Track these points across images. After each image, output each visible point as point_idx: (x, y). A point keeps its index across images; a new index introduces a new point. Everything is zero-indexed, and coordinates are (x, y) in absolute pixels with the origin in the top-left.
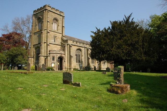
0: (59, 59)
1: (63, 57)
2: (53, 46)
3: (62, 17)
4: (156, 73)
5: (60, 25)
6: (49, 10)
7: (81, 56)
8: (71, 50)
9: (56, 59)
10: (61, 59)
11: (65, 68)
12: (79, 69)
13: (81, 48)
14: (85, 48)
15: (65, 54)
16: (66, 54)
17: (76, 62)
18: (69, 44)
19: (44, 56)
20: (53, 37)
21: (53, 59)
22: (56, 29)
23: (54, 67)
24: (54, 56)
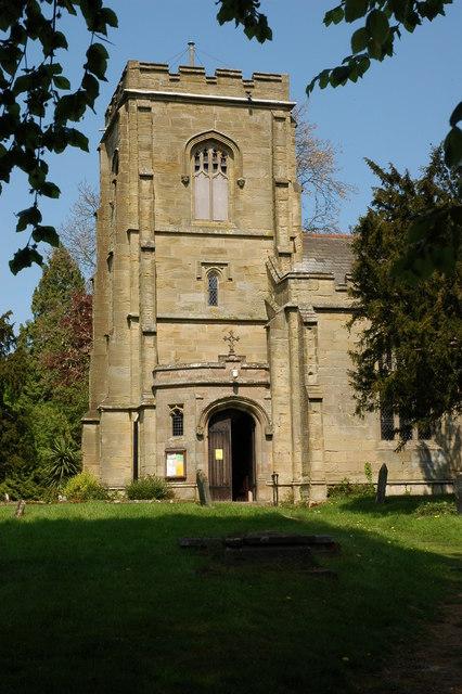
0: (225, 425)
1: (250, 408)
2: (203, 336)
3: (264, 112)
4: (180, 516)
6: (148, 96)
8: (310, 352)
9: (193, 422)
11: (276, 486)
12: (419, 490)
16: (281, 385)
18: (295, 309)
19: (130, 411)
20: (194, 269)
22: (221, 212)
23: (182, 479)
24: (182, 406)
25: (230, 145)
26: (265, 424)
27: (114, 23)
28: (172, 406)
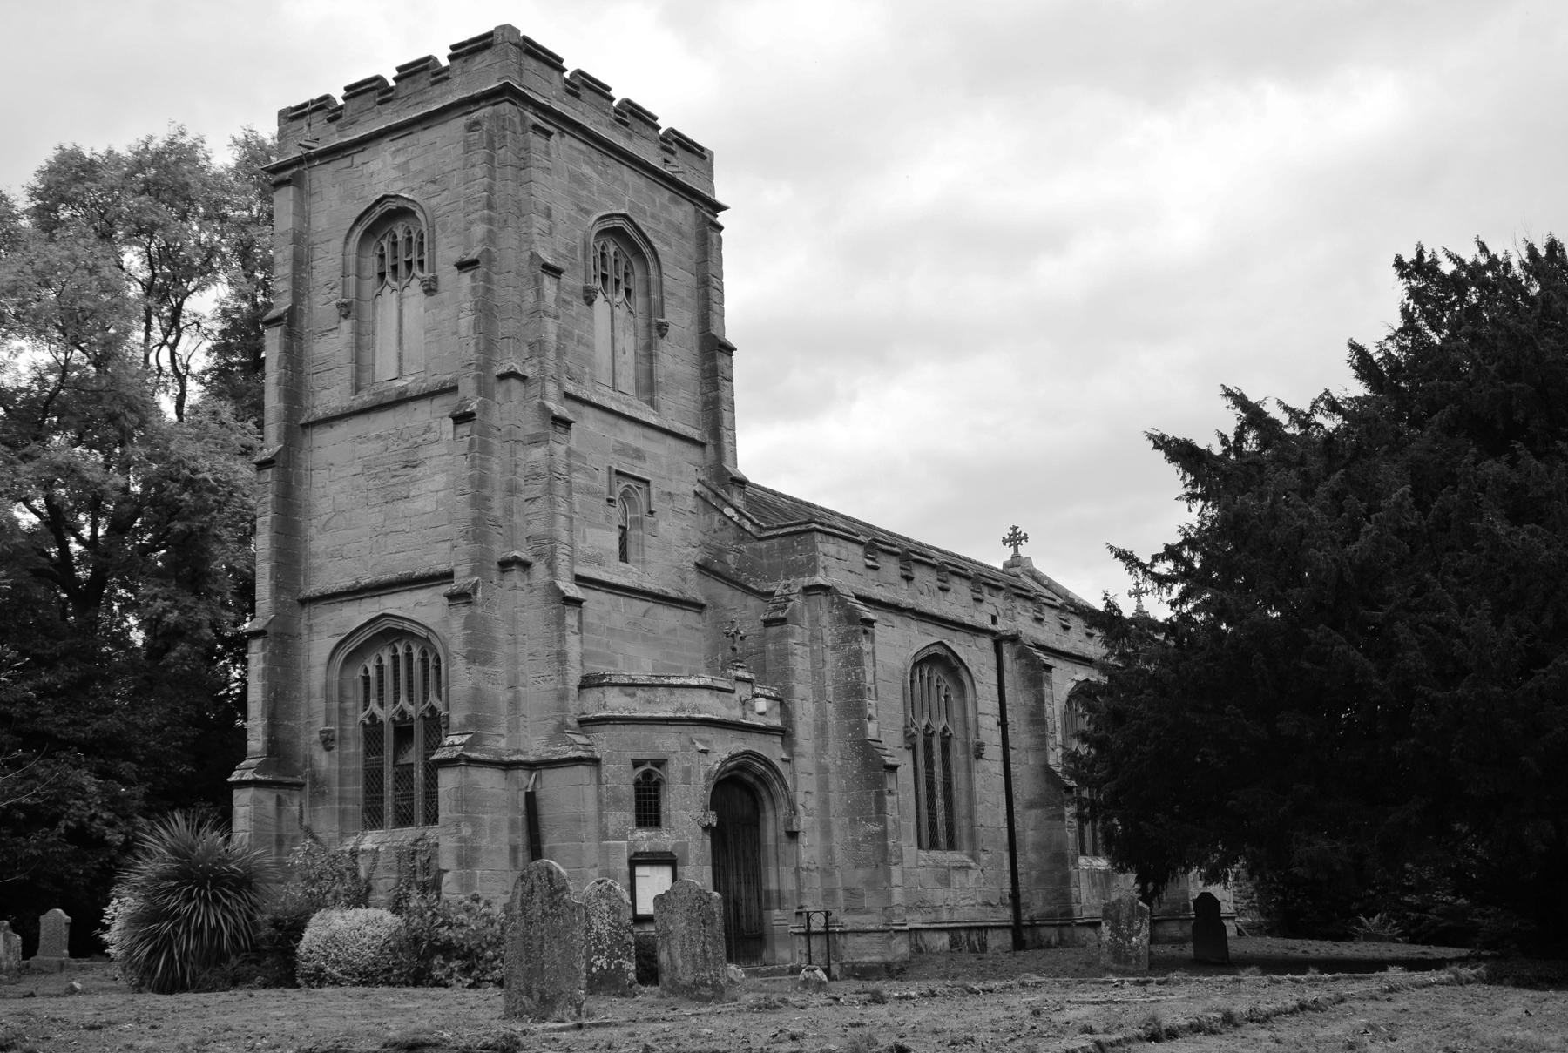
1: (760, 778)
2: (617, 620)
3: (688, 208)
5: (681, 320)
7: (957, 747)
10: (742, 798)
11: (580, 1026)
13: (961, 646)
14: (999, 641)
15: (785, 733)
17: (920, 847)
20: (601, 481)
21: (648, 810)
24: (660, 763)
25: (646, 250)
26: (783, 811)
27: (1399, 263)
28: (637, 764)
